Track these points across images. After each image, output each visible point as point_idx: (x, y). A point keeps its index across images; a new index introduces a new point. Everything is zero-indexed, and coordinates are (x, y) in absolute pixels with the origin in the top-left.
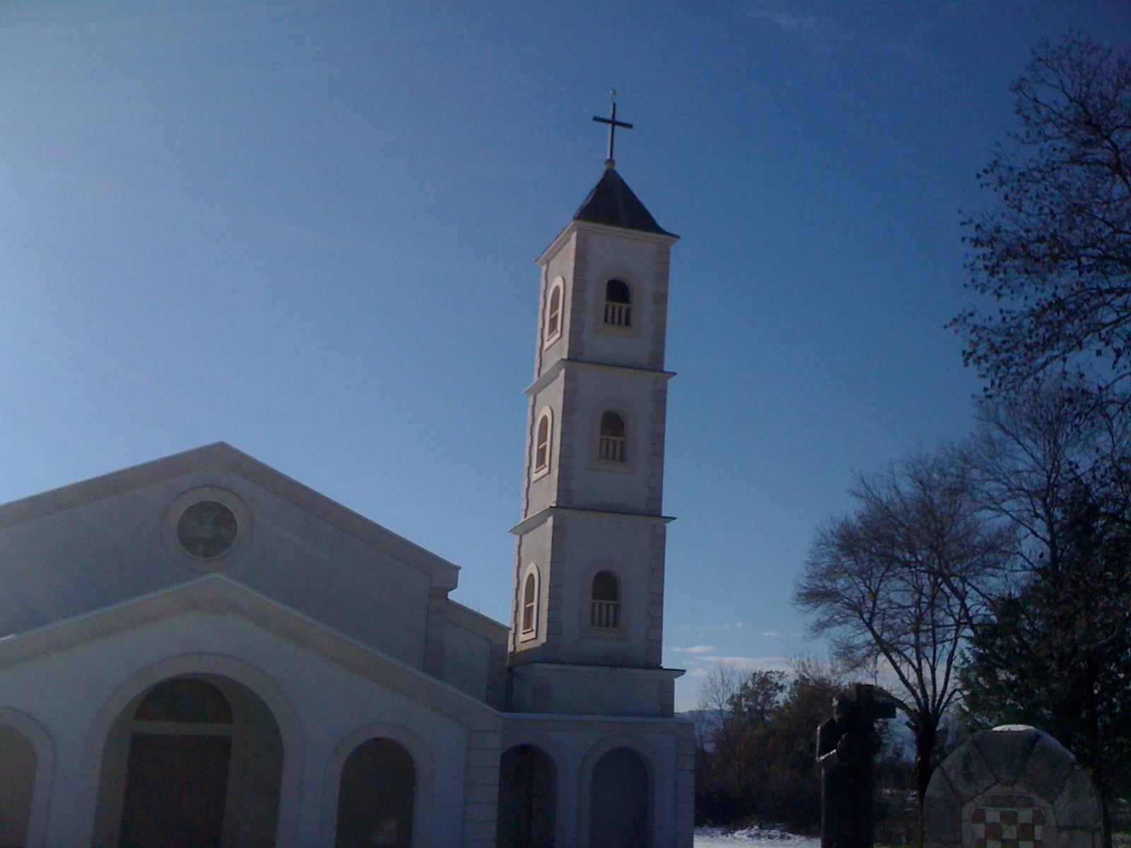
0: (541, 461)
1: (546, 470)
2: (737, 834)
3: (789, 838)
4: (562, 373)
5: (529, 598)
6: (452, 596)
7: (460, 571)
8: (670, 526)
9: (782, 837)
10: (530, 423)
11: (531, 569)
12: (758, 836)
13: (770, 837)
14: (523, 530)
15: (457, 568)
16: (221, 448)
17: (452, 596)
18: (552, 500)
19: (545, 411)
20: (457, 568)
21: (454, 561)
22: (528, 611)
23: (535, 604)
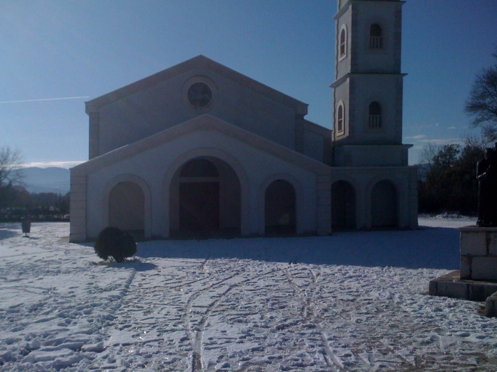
0: (342, 52)
1: (342, 133)
2: (437, 216)
3: (461, 218)
4: (350, 7)
5: (340, 116)
6: (306, 118)
7: (309, 107)
8: (405, 78)
9: (458, 217)
10: (336, 33)
11: (340, 103)
12: (447, 217)
13: (452, 217)
14: (335, 86)
15: (307, 105)
16: (201, 59)
17: (306, 118)
18: (348, 70)
19: (343, 27)
20: (307, 105)
21: (304, 101)
22: (340, 122)
23: (343, 119)
